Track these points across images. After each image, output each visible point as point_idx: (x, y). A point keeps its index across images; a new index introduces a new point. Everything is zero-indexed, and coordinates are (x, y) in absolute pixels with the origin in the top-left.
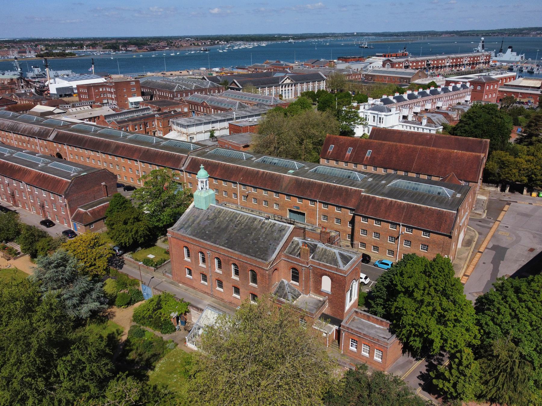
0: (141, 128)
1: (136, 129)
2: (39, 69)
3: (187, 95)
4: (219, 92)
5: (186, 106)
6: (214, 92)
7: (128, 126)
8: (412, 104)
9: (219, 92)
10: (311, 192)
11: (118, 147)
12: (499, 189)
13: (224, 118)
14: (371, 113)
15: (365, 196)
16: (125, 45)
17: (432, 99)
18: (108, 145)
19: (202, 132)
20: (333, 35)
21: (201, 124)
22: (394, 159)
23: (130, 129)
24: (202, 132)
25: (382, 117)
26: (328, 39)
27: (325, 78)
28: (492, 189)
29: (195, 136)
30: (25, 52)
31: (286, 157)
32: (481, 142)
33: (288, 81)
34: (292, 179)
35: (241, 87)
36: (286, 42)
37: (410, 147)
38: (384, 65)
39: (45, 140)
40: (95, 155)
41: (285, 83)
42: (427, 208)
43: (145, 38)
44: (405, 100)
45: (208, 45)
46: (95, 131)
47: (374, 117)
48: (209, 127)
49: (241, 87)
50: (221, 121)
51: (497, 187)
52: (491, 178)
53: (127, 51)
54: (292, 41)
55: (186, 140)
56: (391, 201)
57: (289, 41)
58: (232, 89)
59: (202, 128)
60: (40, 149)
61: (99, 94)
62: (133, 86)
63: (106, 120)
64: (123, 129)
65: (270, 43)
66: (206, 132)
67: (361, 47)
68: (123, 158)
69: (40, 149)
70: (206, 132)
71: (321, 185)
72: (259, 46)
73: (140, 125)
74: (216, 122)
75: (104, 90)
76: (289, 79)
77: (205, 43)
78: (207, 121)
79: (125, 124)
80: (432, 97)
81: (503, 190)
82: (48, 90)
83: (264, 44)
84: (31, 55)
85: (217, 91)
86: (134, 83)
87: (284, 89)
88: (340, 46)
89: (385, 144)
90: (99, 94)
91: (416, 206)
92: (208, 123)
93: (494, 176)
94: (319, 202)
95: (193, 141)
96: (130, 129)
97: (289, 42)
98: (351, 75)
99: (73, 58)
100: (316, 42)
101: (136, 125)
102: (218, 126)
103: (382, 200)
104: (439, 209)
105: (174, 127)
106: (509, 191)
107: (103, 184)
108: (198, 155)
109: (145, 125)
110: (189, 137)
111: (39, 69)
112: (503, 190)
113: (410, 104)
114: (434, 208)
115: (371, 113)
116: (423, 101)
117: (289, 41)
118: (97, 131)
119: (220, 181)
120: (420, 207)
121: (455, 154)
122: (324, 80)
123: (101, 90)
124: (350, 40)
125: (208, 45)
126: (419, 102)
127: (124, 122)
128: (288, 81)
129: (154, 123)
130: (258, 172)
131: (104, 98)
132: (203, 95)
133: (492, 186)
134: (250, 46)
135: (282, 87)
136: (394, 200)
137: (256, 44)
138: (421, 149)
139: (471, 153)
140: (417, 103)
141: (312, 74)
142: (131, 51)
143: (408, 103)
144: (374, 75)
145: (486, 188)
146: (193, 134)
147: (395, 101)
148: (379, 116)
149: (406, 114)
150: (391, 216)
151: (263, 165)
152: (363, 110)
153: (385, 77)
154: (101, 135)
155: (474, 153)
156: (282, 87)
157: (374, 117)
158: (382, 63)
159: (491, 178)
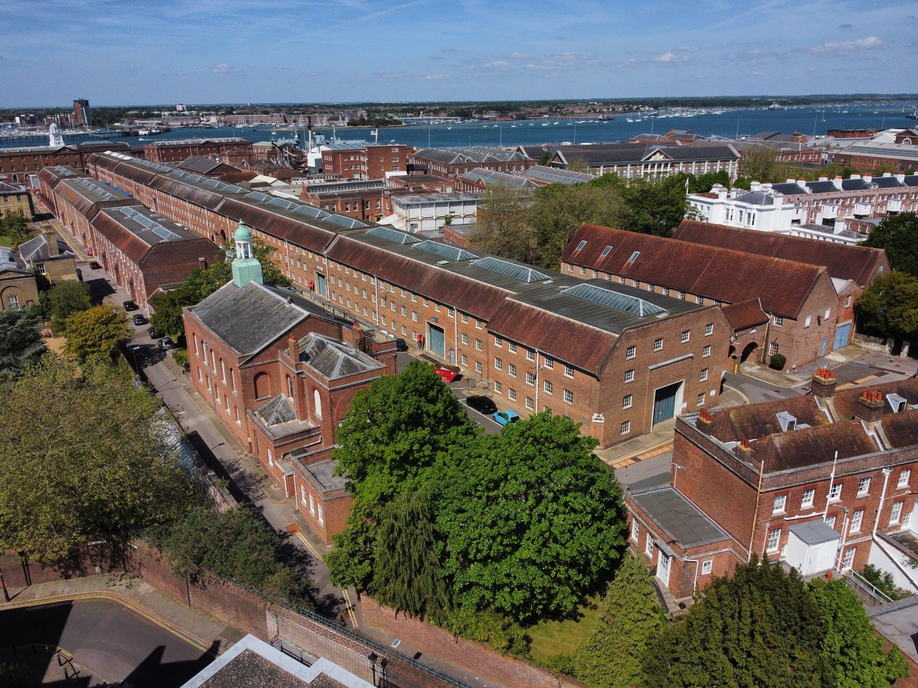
0: (355, 208)
1: (347, 209)
2: (323, 137)
3: (462, 172)
4: (527, 168)
5: (449, 184)
6: (518, 169)
7: (335, 203)
8: (852, 198)
9: (527, 168)
10: (451, 294)
11: (276, 221)
12: (887, 348)
13: (472, 199)
14: (736, 206)
15: (509, 301)
16: (480, 111)
17: (908, 194)
18: (265, 217)
19: (431, 218)
20: (873, 98)
21: (431, 205)
22: (670, 268)
23: (338, 207)
24: (431, 218)
25: (753, 212)
26: (856, 104)
27: (739, 155)
28: (874, 347)
29: (419, 223)
30: (337, 119)
31: (510, 257)
32: (867, 252)
33: (659, 157)
34: (437, 272)
35: (566, 163)
36: (765, 108)
37: (702, 249)
38: (899, 140)
39: (318, 254)
40: (336, 268)
41: (652, 159)
42: (582, 326)
43: (516, 102)
44: (835, 190)
45: (620, 112)
46: (409, 244)
47: (741, 212)
48: (445, 211)
49: (566, 163)
50: (466, 203)
51: (884, 344)
52: (868, 324)
53: (481, 119)
54: (776, 106)
55: (404, 229)
56: (539, 312)
57: (772, 107)
58: (554, 165)
59: (431, 211)
60: (379, 303)
61: (349, 164)
62: (396, 155)
63: (309, 194)
64: (327, 208)
65: (731, 109)
66: (438, 218)
67: (911, 117)
68: (415, 294)
69: (379, 303)
70: (438, 218)
71: (468, 284)
72: (709, 115)
73: (355, 203)
74: (458, 203)
75: (352, 159)
76: (661, 154)
77: (614, 109)
78: (441, 201)
79: (331, 200)
80: (907, 189)
81: (896, 351)
82: (306, 161)
83: (718, 112)
84: (343, 124)
85: (523, 168)
86: (397, 150)
87: (649, 171)
88: (872, 115)
89: (664, 242)
90: (349, 164)
91: (569, 322)
92: (445, 204)
93: (877, 321)
94: (458, 311)
95: (416, 231)
96: (338, 207)
97: (771, 109)
98: (798, 153)
99: (398, 127)
100: (822, 109)
101: (347, 203)
102: (459, 210)
103: (528, 310)
104: (598, 329)
105: (397, 208)
106: (910, 354)
107: (202, 259)
108: (348, 236)
109: (364, 205)
110: (409, 224)
111: (323, 137)
112: (896, 351)
113: (845, 199)
114: (591, 327)
115: (736, 206)
116: (883, 196)
117: (772, 107)
118: (411, 244)
119: (470, 318)
120: (574, 324)
121: (773, 266)
122: (734, 158)
123: (352, 159)
124: (896, 107)
125: (620, 112)
126: (871, 197)
127: (333, 196)
128: (659, 157)
129: (379, 203)
130: (403, 260)
131: (356, 172)
132: (500, 174)
133: (875, 342)
134: (688, 113)
135: (646, 167)
136: (544, 311)
137: (704, 111)
138: (720, 253)
139: (802, 264)
140: (865, 197)
141: (712, 148)
142: (488, 119)
143: (838, 195)
144: (850, 156)
145: (864, 345)
146: (416, 219)
147: (807, 189)
148: (749, 211)
149: (830, 216)
150: (529, 337)
151: (481, 273)
152: (724, 201)
153: (871, 159)
154: (418, 253)
155: (807, 265)
156: (646, 167)
157: (741, 212)
158: (894, 139)
159: (868, 324)
